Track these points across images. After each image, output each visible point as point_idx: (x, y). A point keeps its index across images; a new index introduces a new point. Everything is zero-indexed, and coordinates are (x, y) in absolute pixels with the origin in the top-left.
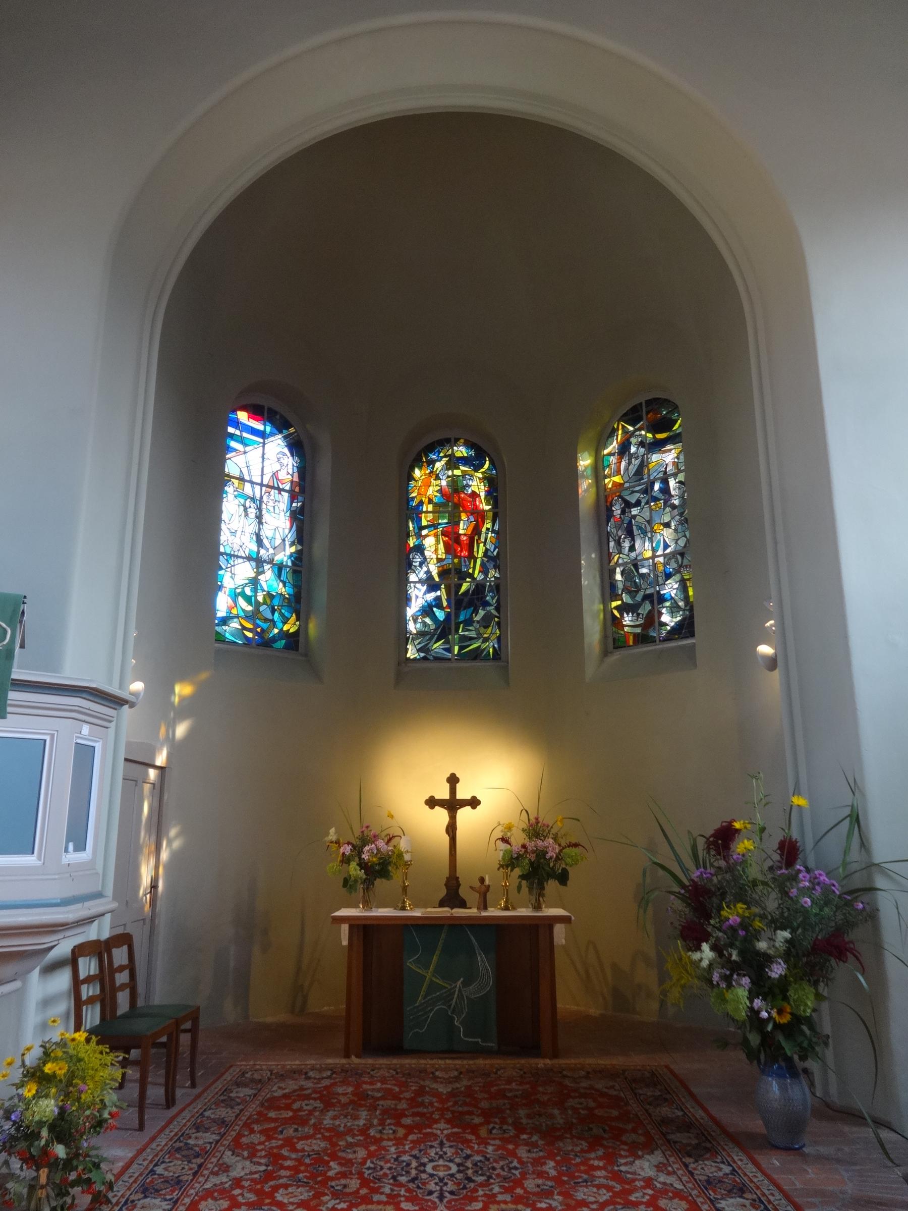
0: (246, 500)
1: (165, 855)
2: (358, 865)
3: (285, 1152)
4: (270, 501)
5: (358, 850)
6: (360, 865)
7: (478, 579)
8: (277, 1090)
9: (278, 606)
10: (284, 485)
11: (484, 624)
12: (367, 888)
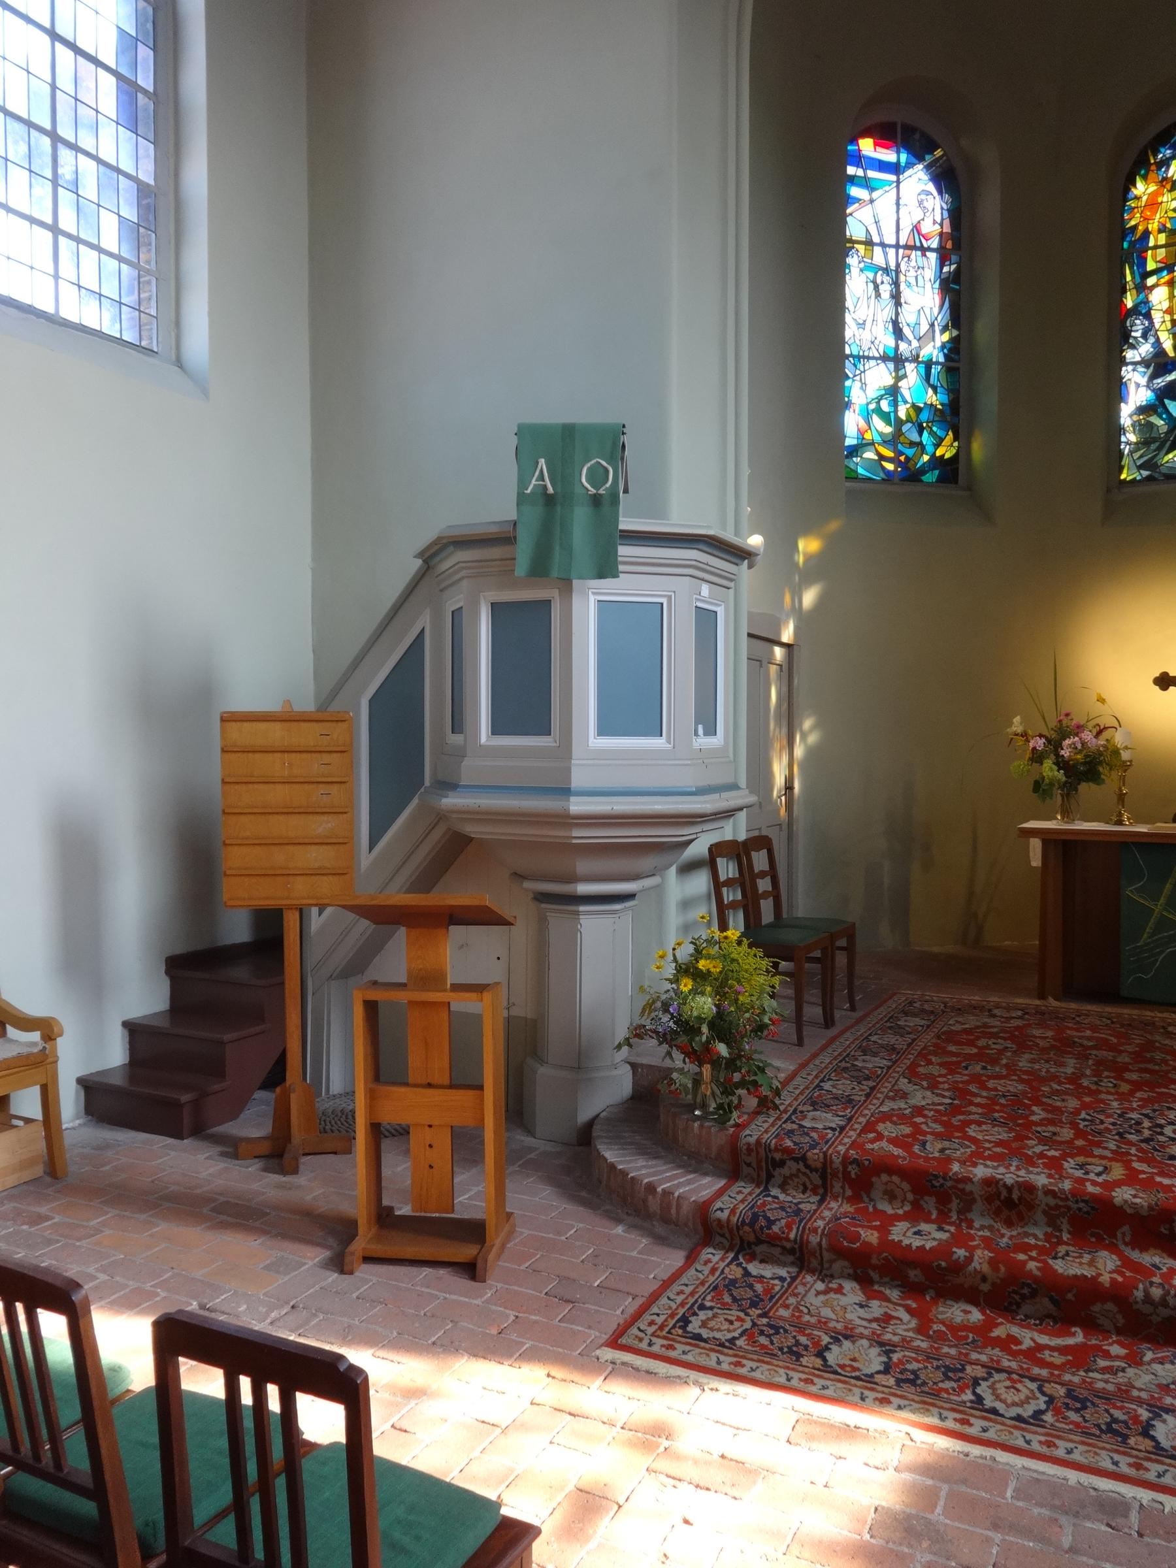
0: (876, 274)
1: (799, 751)
2: (1054, 763)
3: (973, 1088)
4: (911, 269)
5: (1055, 745)
6: (1057, 764)
8: (954, 1024)
10: (929, 242)
12: (1068, 795)
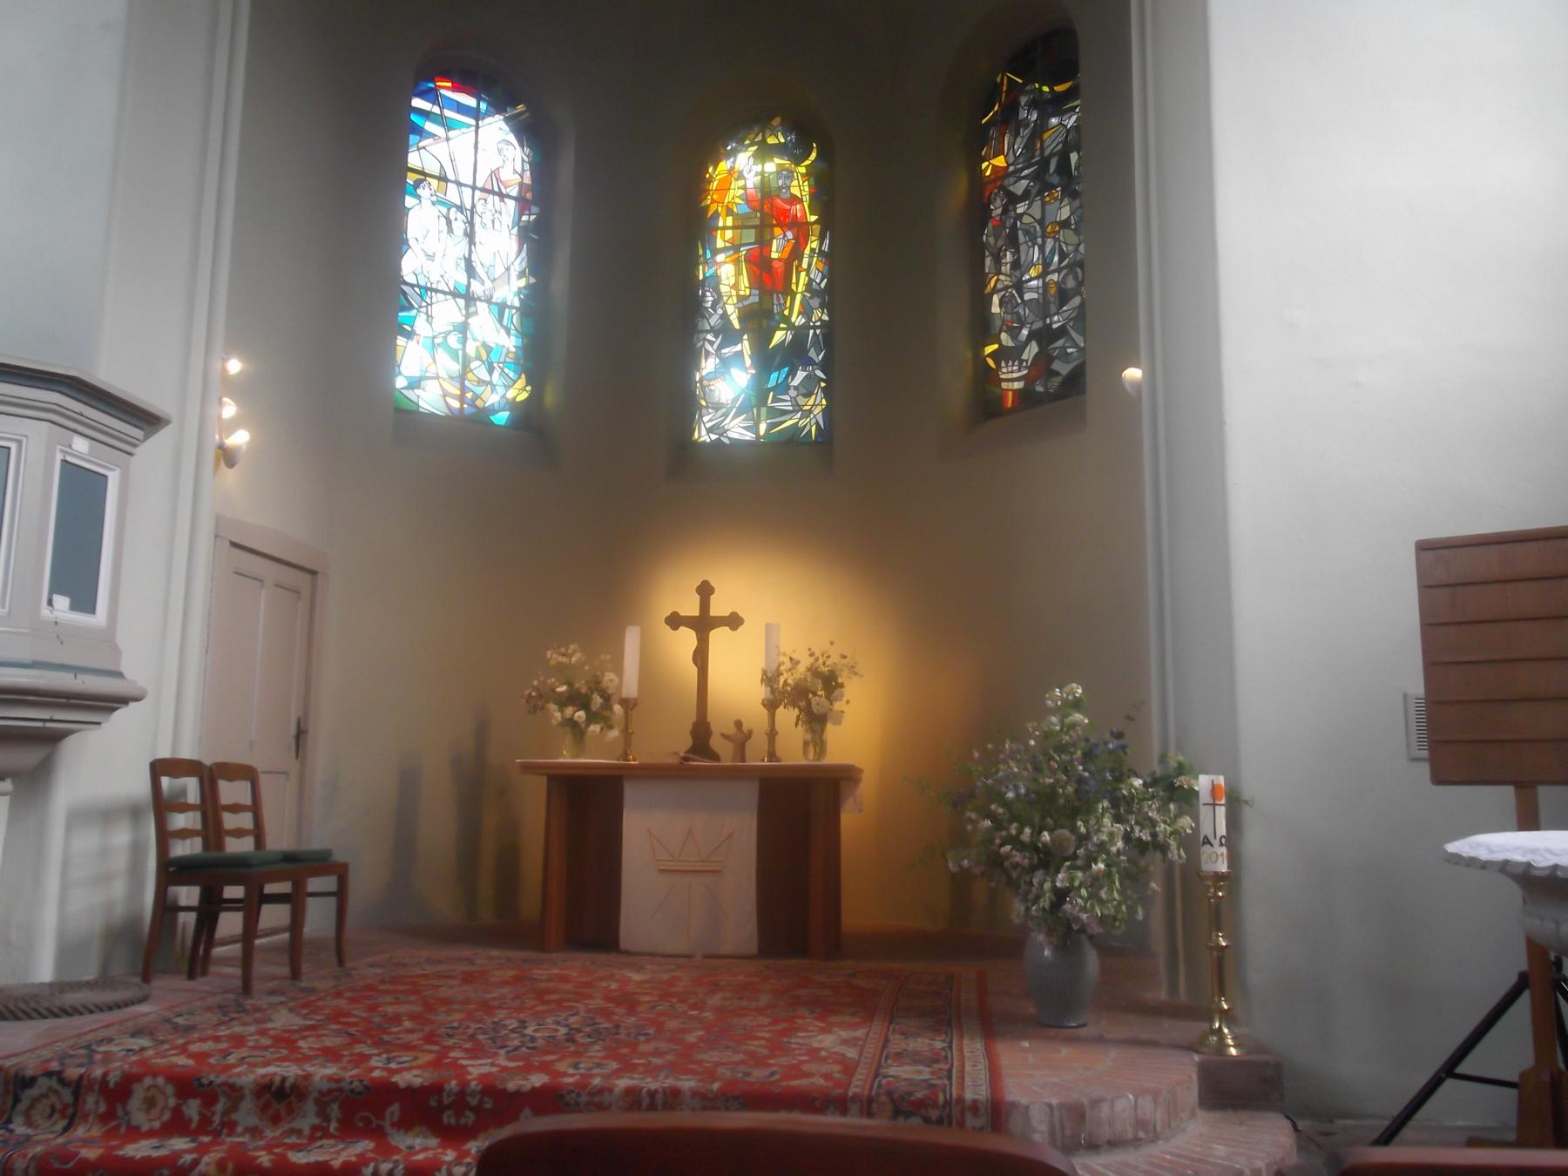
4: (487, 212)
7: (796, 324)
9: (498, 363)
10: (508, 190)
11: (804, 391)
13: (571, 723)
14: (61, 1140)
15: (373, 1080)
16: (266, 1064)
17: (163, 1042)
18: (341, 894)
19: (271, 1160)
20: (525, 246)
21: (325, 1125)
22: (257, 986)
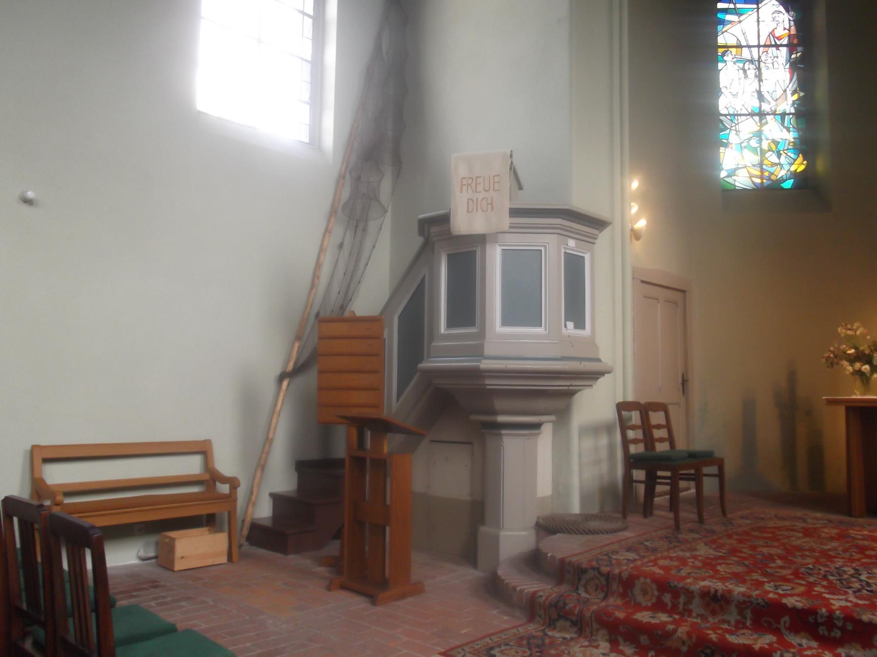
10: (781, 41)
13: (860, 373)
14: (603, 604)
15: (770, 599)
16: (703, 579)
17: (644, 557)
18: (721, 475)
19: (716, 637)
20: (795, 73)
21: (744, 621)
22: (682, 526)
